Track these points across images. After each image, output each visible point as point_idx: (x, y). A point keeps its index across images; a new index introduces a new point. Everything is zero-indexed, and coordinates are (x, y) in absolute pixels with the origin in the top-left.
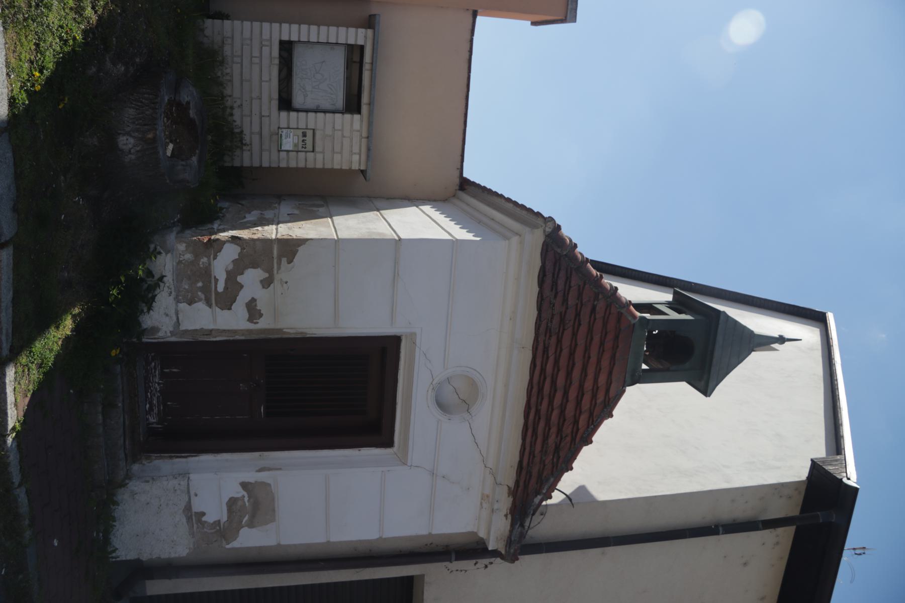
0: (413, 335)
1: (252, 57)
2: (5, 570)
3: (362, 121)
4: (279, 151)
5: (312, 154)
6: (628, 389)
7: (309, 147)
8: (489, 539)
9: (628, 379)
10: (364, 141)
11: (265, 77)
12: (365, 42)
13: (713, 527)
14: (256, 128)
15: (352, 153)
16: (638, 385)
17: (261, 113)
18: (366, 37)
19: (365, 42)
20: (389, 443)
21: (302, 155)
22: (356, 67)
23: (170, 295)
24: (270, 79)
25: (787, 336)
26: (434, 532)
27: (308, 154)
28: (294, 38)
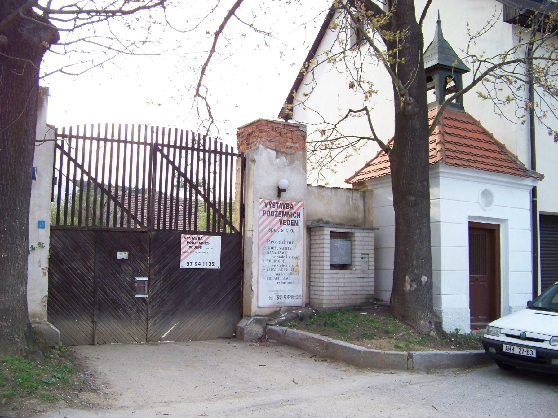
0: (470, 217)
1: (336, 282)
2: (138, 294)
3: (357, 232)
4: (369, 270)
5: (370, 255)
6: (466, 111)
7: (366, 256)
8: (532, 186)
9: (462, 111)
10: (364, 231)
11: (343, 276)
12: (329, 231)
13: (42, 15)
14: (361, 280)
15: (369, 237)
16: (464, 105)
17: (356, 278)
18: (327, 231)
19: (329, 231)
20: (499, 226)
21: (370, 259)
22: (151, 205)
23: (39, 244)
24: (344, 274)
25: (437, 19)
26: (529, 209)
27: (370, 256)
28: (329, 263)
